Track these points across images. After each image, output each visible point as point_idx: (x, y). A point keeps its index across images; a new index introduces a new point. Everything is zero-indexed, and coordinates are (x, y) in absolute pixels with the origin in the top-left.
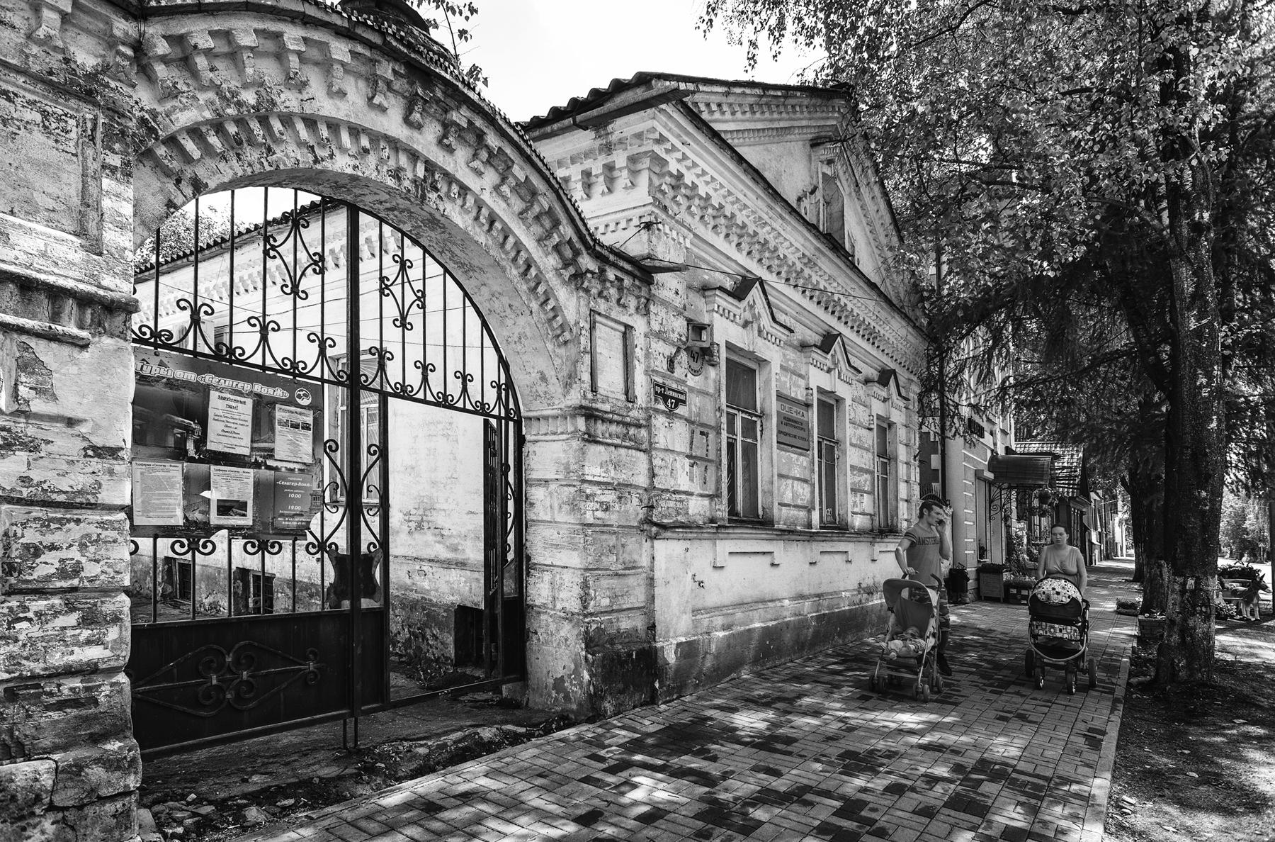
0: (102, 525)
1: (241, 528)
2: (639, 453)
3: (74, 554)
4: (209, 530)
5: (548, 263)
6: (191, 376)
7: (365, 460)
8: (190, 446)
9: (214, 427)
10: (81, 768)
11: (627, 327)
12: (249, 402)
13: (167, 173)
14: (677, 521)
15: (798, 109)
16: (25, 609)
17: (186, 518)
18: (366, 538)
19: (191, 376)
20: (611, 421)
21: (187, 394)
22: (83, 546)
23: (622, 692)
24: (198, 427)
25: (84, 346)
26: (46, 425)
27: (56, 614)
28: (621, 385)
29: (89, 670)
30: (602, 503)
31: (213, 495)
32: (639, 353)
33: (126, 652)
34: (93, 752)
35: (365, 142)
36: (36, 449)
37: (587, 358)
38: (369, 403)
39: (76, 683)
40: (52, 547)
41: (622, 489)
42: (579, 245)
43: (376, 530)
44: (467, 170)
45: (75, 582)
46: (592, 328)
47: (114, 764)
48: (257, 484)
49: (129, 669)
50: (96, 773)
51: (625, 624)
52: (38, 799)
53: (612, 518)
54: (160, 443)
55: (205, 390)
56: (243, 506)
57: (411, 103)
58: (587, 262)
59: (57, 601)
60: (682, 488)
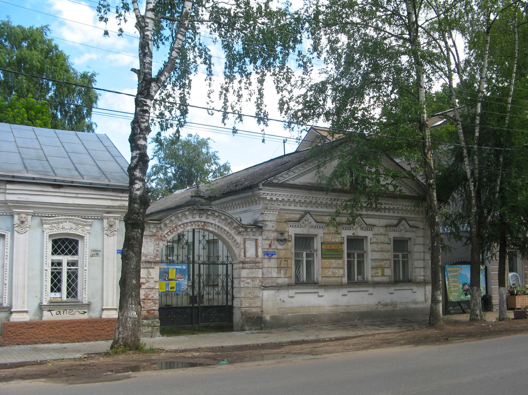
0: (156, 291)
5: (232, 232)
6: (166, 267)
7: (196, 277)
9: (170, 275)
11: (256, 239)
15: (169, 233)
18: (196, 293)
19: (166, 267)
20: (250, 263)
25: (154, 268)
28: (255, 253)
29: (154, 310)
30: (247, 282)
32: (260, 245)
33: (158, 308)
35: (192, 223)
37: (243, 250)
38: (196, 266)
41: (253, 279)
42: (239, 226)
43: (198, 291)
46: (244, 242)
47: (157, 322)
49: (159, 310)
50: (155, 323)
51: (254, 310)
53: (250, 285)
55: (169, 268)
57: (200, 214)
58: (241, 229)
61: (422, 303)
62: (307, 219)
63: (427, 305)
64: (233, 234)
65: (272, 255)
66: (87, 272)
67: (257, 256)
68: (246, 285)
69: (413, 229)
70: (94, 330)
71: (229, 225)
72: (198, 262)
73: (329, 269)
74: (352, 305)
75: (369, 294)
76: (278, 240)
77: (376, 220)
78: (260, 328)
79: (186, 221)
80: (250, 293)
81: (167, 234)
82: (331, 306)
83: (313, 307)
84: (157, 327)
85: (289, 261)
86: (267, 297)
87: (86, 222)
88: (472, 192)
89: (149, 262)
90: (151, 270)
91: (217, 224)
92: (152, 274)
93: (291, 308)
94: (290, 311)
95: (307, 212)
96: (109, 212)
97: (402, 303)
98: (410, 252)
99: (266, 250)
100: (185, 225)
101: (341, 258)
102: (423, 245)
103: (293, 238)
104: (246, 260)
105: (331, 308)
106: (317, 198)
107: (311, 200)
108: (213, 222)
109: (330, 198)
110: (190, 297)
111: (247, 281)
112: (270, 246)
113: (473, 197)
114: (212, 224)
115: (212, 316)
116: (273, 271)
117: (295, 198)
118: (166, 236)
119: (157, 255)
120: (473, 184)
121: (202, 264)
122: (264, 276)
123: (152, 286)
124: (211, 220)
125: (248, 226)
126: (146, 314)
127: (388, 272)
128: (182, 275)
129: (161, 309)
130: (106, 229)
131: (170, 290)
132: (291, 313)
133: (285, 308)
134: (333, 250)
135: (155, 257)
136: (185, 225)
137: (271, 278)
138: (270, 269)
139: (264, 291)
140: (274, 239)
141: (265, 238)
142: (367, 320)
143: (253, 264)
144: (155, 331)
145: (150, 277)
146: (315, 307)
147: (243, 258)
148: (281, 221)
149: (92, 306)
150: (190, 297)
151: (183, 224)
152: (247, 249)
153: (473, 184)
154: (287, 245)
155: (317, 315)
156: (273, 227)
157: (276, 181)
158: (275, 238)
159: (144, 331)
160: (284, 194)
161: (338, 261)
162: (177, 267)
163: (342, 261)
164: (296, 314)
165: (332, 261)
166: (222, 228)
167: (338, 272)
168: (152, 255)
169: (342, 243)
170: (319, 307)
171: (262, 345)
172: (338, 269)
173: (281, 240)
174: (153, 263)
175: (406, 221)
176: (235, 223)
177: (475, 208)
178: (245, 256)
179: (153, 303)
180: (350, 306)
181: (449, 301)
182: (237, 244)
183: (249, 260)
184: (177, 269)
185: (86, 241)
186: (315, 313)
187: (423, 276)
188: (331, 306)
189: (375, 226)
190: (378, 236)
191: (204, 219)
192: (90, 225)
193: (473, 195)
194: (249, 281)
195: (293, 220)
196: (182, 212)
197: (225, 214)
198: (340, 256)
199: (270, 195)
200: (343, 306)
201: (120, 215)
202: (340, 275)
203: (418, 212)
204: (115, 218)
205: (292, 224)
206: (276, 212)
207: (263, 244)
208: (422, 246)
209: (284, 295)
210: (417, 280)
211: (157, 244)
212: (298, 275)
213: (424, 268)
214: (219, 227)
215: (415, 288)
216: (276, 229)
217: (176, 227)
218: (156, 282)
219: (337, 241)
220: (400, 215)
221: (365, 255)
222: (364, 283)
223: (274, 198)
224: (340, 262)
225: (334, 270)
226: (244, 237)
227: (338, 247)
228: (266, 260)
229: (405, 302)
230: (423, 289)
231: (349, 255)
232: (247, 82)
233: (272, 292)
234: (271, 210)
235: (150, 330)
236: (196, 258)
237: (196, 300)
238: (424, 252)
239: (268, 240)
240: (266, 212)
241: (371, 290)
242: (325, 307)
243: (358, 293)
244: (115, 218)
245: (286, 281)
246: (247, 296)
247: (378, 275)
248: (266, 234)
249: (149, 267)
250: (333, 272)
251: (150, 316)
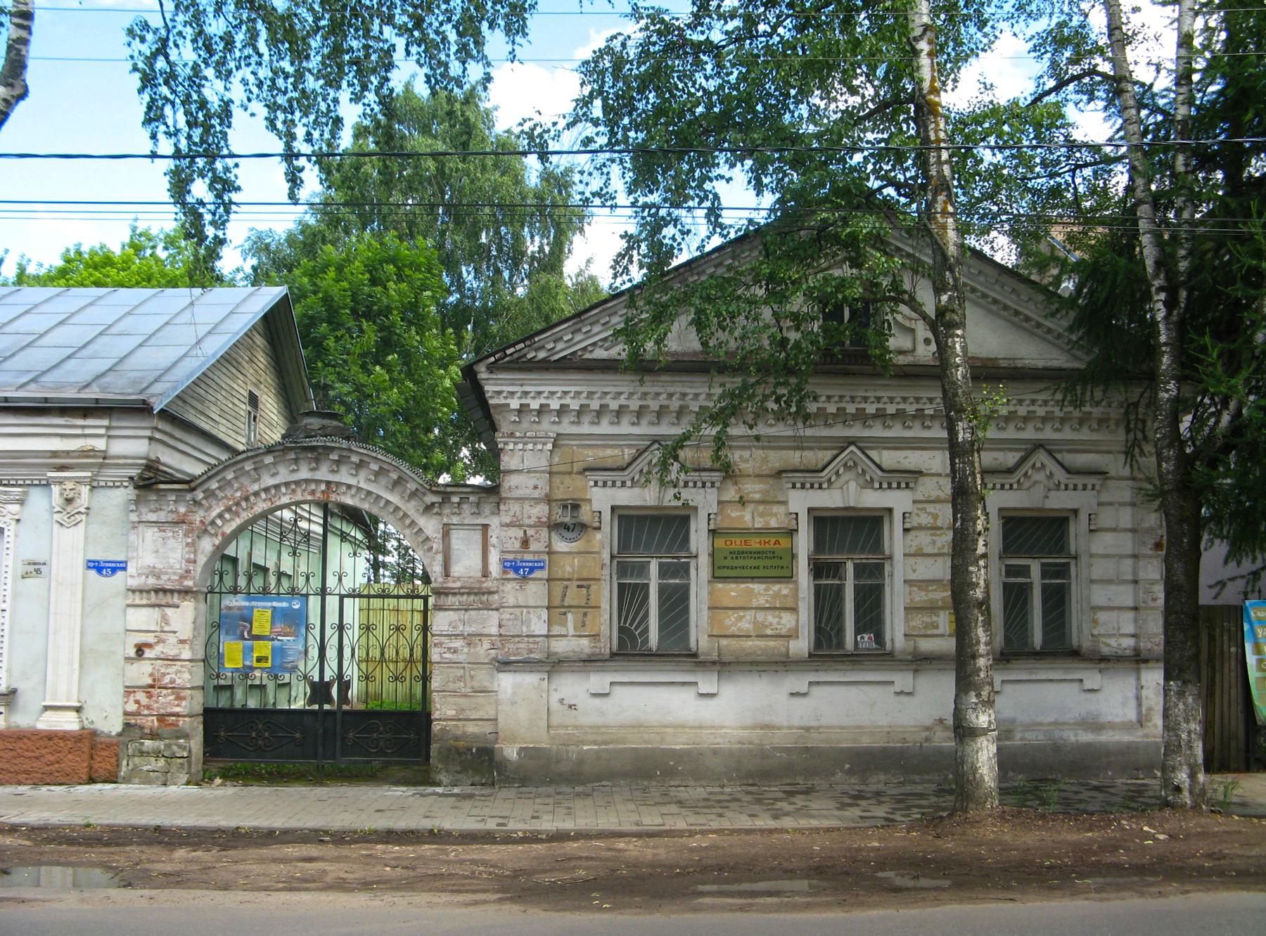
6: (247, 604)
9: (255, 624)
13: (212, 535)
15: (227, 516)
19: (247, 604)
23: (458, 772)
25: (178, 607)
28: (480, 566)
29: (177, 715)
30: (449, 649)
32: (493, 540)
34: (174, 741)
35: (293, 486)
38: (332, 602)
48: (273, 649)
50: (175, 748)
51: (471, 728)
53: (461, 657)
54: (234, 634)
56: (267, 658)
61: (1127, 727)
62: (1039, 465)
63: (1146, 736)
64: (411, 512)
65: (532, 570)
66: (6, 614)
67: (486, 574)
68: (446, 656)
69: (1081, 481)
70: (15, 758)
71: (398, 489)
72: (337, 592)
73: (741, 613)
74: (829, 727)
75: (897, 694)
76: (554, 527)
77: (927, 455)
80: (460, 679)
81: (220, 516)
82: (744, 728)
83: (675, 727)
84: (179, 761)
86: (514, 693)
87: (6, 493)
88: (1162, 327)
89: (165, 591)
90: (169, 611)
91: (362, 485)
92: (172, 623)
94: (590, 738)
95: (1039, 445)
96: (62, 468)
97: (1040, 724)
98: (1076, 558)
99: (510, 557)
101: (788, 577)
102: (1133, 531)
103: (607, 516)
104: (451, 585)
105: (742, 733)
106: (684, 395)
107: (666, 403)
108: (352, 481)
110: (313, 685)
111: (452, 645)
113: (1165, 344)
114: (349, 487)
117: (608, 400)
118: (219, 522)
120: (1162, 296)
121: (349, 596)
123: (171, 651)
124: (344, 476)
125: (449, 489)
126: (156, 724)
127: (605, 619)
128: (290, 627)
129: (210, 715)
130: (58, 509)
131: (255, 664)
132: (595, 743)
133: (575, 727)
134: (759, 554)
135: (182, 577)
139: (502, 675)
140: (538, 524)
141: (507, 520)
142: (882, 777)
145: (166, 629)
146: (683, 727)
147: (440, 580)
149: (22, 699)
150: (313, 685)
151: (266, 490)
152: (455, 555)
153: (1162, 296)
154: (588, 541)
155: (688, 753)
157: (542, 355)
158: (544, 519)
159: (145, 768)
161: (776, 587)
162: (275, 604)
163: (791, 586)
164: (611, 746)
165: (751, 586)
166: (379, 497)
167: (775, 621)
168: (174, 574)
169: (792, 532)
170: (700, 727)
171: (285, 832)
172: (777, 613)
174: (176, 595)
175: (1050, 453)
177: (1171, 386)
179: (172, 697)
180: (819, 728)
181: (1259, 723)
182: (427, 539)
183: (458, 584)
184: (274, 608)
185: (6, 539)
186: (678, 747)
187: (1133, 636)
188: (744, 728)
189: (920, 473)
190: (938, 506)
191: (323, 473)
192: (21, 502)
193: (1163, 339)
194: (458, 644)
198: (786, 573)
199: (836, 399)
200: (789, 728)
201: (89, 474)
202: (783, 632)
203: (1101, 421)
204: (79, 481)
205: (600, 476)
206: (544, 444)
207: (504, 539)
208: (1130, 535)
209: (573, 687)
210: (1105, 651)
212: (636, 629)
213: (1136, 609)
214: (369, 493)
215: (1092, 678)
216: (546, 495)
217: (247, 499)
218: (182, 642)
219: (773, 523)
220: (1029, 434)
221: (887, 568)
222: (882, 657)
223: (851, 409)
224: (785, 592)
225: (761, 616)
226: (445, 520)
227: (777, 542)
228: (509, 586)
229: (1050, 724)
230: (1131, 680)
231: (819, 569)
232: (290, 69)
233: (530, 680)
236: (331, 582)
238: (1135, 556)
239: (520, 526)
240: (511, 446)
241: (903, 680)
242: (722, 727)
243: (853, 689)
244: (79, 481)
245: (584, 646)
246: (451, 686)
247: (936, 632)
248: (510, 511)
250: (755, 622)
251: (166, 731)
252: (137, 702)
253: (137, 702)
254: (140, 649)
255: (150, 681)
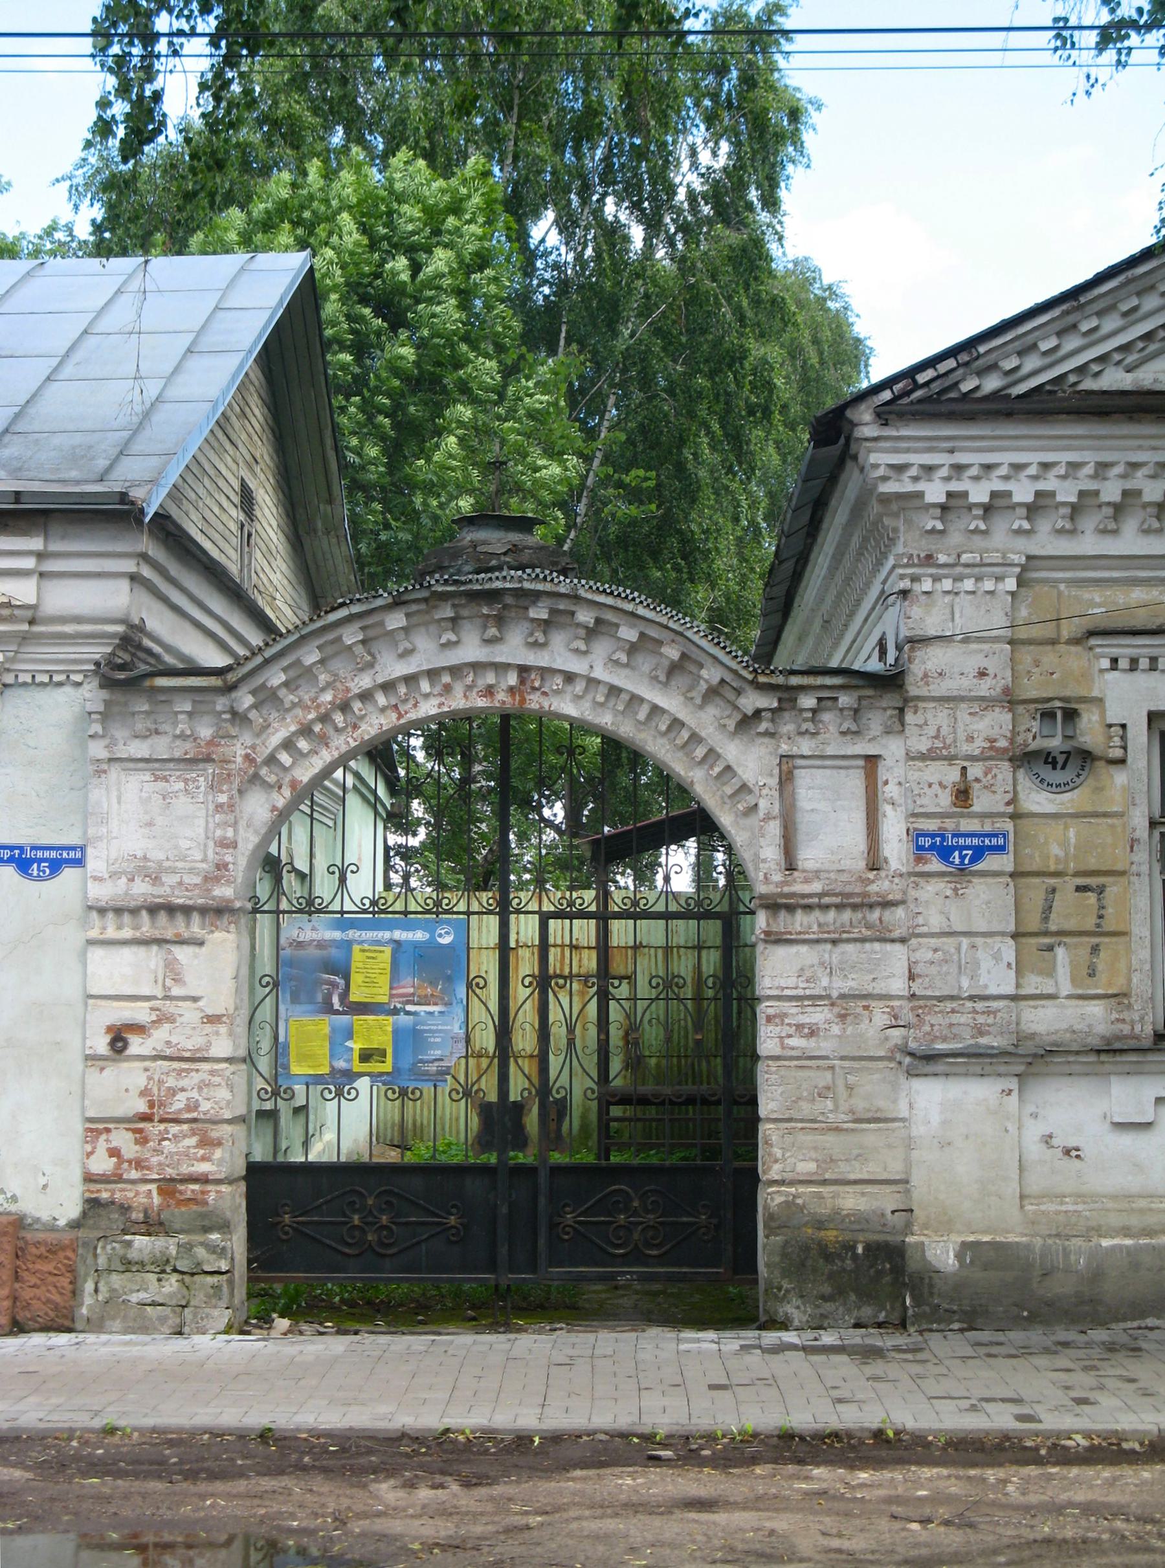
0: (212, 1073)
1: (382, 1074)
2: (889, 947)
3: (194, 1094)
4: (351, 1076)
6: (337, 935)
7: (521, 993)
8: (335, 1000)
9: (356, 979)
10: (192, 1247)
11: (868, 758)
12: (388, 951)
14: (977, 1045)
15: (303, 744)
16: (167, 1132)
17: (332, 1067)
18: (518, 1087)
19: (337, 935)
20: (826, 907)
21: (333, 952)
22: (200, 1089)
23: (825, 1298)
24: (342, 982)
25: (201, 944)
26: (180, 1004)
27: (185, 1136)
30: (799, 1027)
31: (356, 1045)
32: (891, 790)
35: (446, 679)
36: (173, 1021)
37: (774, 829)
39: (196, 1187)
40: (183, 1090)
44: (569, 654)
45: (195, 1115)
46: (786, 779)
48: (396, 1032)
50: (201, 1252)
51: (851, 1201)
52: (168, 1261)
53: (825, 1046)
54: (311, 1001)
55: (348, 945)
56: (383, 1053)
59: (185, 1127)
60: (993, 990)
65: (979, 853)
67: (875, 864)
68: (792, 1042)
71: (680, 681)
78: (895, 1318)
79: (395, 668)
80: (824, 1093)
81: (288, 745)
85: (1114, 889)
86: (944, 1123)
89: (171, 909)
90: (182, 954)
91: (599, 673)
92: (188, 977)
93: (1130, 1197)
94: (1115, 1220)
99: (931, 825)
100: (402, 690)
109: (1090, 457)
112: (963, 795)
114: (569, 677)
115: (628, 1228)
116: (980, 954)
117: (1138, 480)
118: (285, 758)
119: (222, 866)
122: (917, 988)
123: (189, 1042)
125: (795, 681)
126: (156, 1200)
128: (433, 984)
132: (1126, 1232)
133: (1080, 1197)
136: (402, 690)
137: (972, 998)
138: (965, 942)
139: (917, 1084)
140: (991, 754)
141: (923, 746)
143: (847, 915)
144: (198, 1299)
145: (176, 991)
147: (777, 877)
148: (1048, 631)
152: (804, 822)
154: (1099, 790)
156: (982, 674)
157: (992, 383)
158: (1003, 743)
159: (135, 1298)
160: (1049, 457)
162: (398, 935)
166: (635, 700)
168: (191, 871)
171: (555, 1439)
173: (1049, 759)
176: (708, 662)
178: (791, 867)
179: (193, 1141)
182: (744, 788)
183: (816, 887)
184: (398, 943)
194: (818, 1016)
195: (1138, 622)
196: (360, 616)
197: (633, 614)
205: (1125, 648)
206: (999, 579)
211: (219, 807)
214: (614, 691)
216: (1007, 691)
217: (345, 707)
218: (212, 1019)
226: (784, 748)
228: (931, 889)
234: (957, 569)
235: (171, 1295)
237: (519, 1128)
239: (950, 759)
240: (927, 585)
246: (806, 1109)
249: (169, 934)
251: (178, 1215)
252: (114, 1152)
253: (114, 1152)
254: (119, 1038)
255: (142, 1107)
